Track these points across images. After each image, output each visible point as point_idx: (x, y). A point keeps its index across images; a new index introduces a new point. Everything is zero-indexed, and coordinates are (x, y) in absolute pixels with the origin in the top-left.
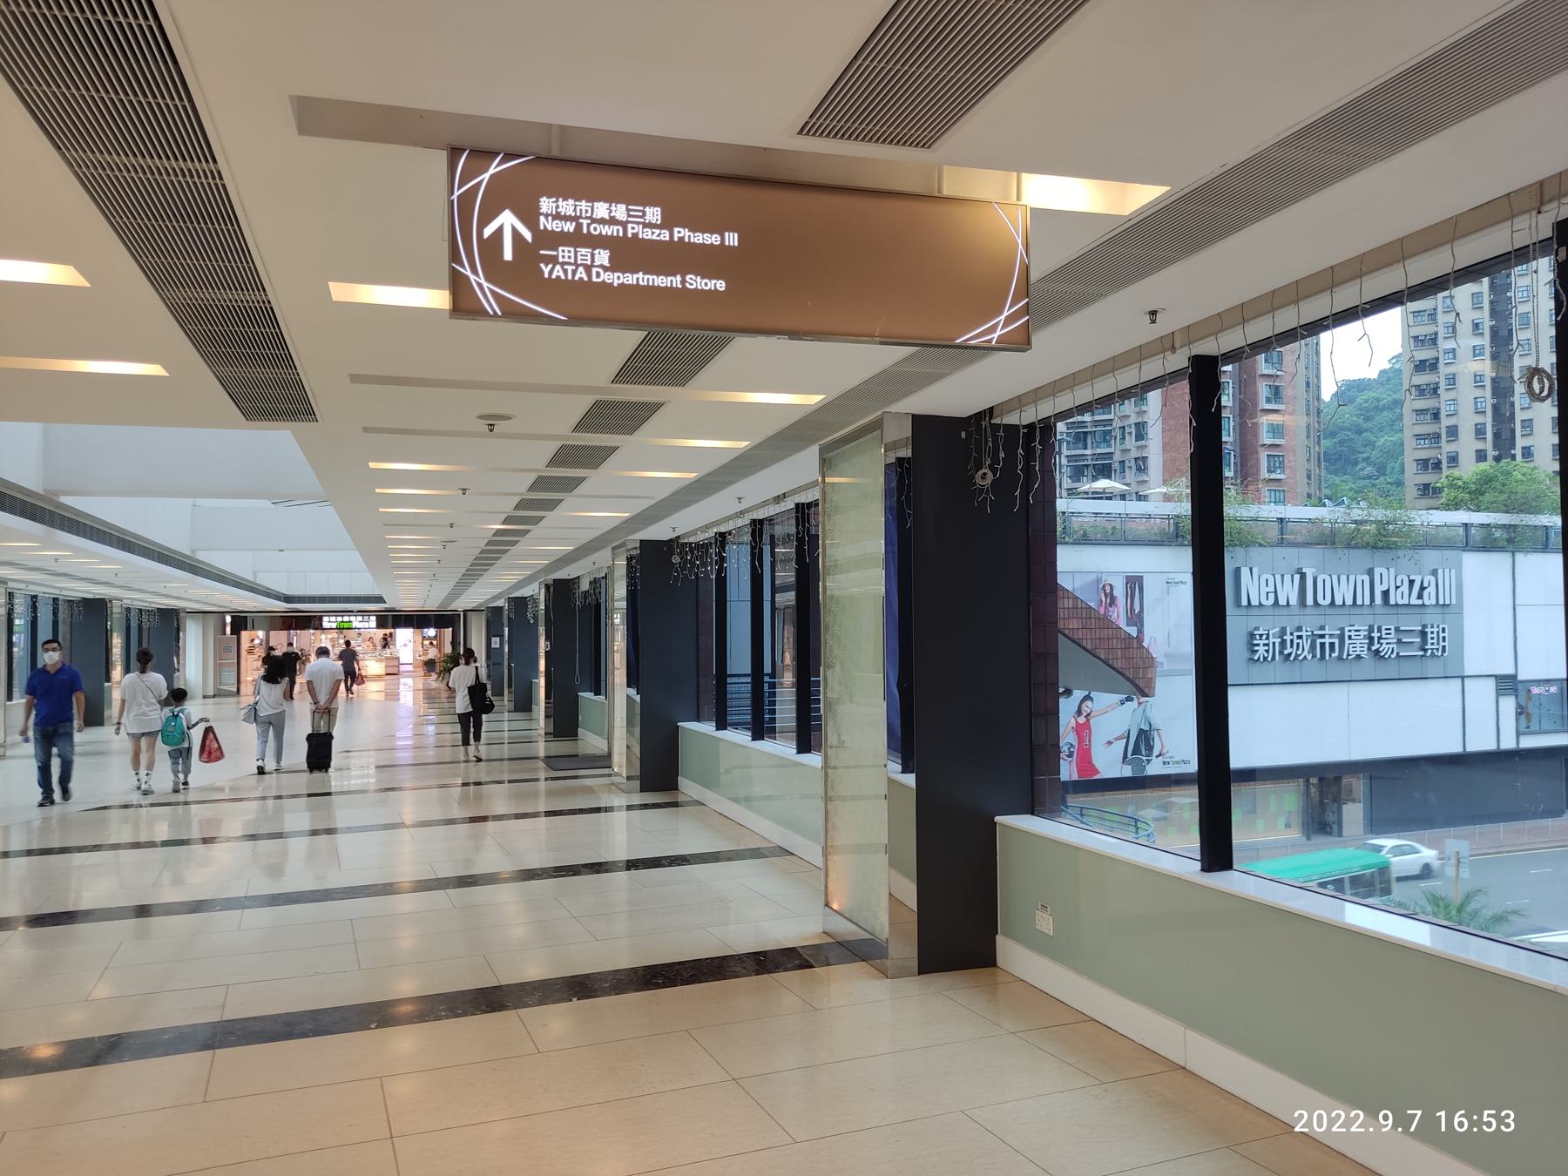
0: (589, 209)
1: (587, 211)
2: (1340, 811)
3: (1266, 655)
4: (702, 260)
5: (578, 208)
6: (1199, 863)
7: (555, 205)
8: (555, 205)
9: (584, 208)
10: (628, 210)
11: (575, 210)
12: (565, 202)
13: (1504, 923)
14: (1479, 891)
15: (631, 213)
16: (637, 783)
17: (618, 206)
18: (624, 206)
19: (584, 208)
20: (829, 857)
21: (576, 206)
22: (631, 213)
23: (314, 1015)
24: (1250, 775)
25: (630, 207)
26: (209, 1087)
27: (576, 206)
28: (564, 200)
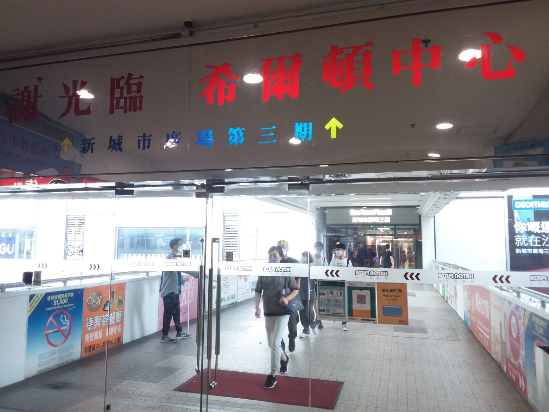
0: (531, 251)
1: (531, 252)
2: (340, 238)
3: (521, 243)
4: (548, 250)
5: (528, 251)
6: (216, 283)
7: (520, 251)
8: (520, 251)
9: (530, 251)
10: (544, 250)
11: (527, 251)
12: (524, 250)
13: (121, 338)
14: (373, 370)
15: (545, 251)
16: (189, 35)
17: (541, 249)
18: (543, 249)
19: (530, 251)
20: (106, 393)
21: (527, 250)
22: (545, 251)
23: (471, 7)
24: (142, 137)
25: (545, 250)
26: (15, 249)
27: (527, 250)
28: (523, 249)
